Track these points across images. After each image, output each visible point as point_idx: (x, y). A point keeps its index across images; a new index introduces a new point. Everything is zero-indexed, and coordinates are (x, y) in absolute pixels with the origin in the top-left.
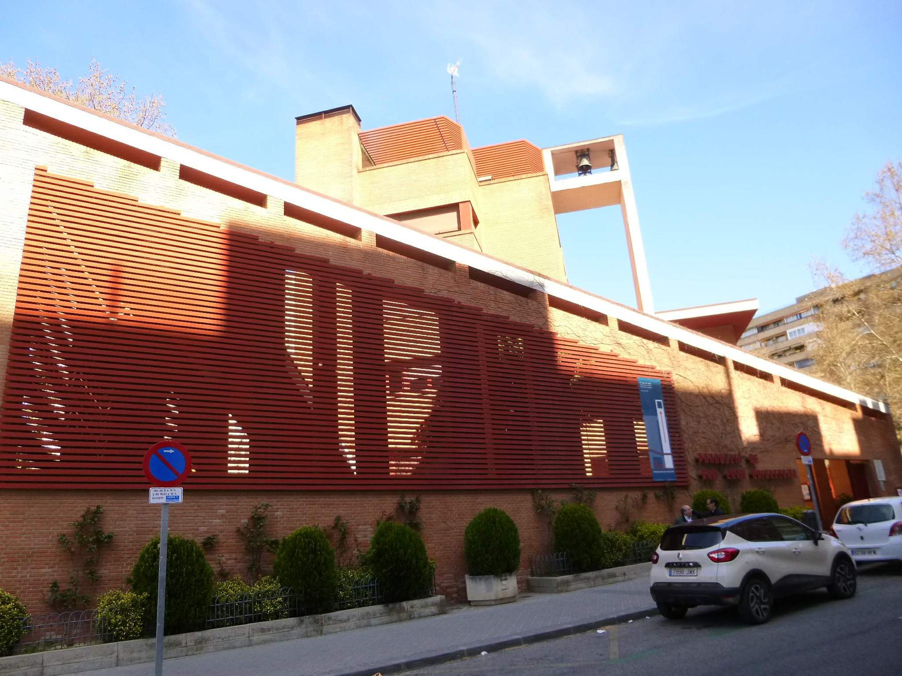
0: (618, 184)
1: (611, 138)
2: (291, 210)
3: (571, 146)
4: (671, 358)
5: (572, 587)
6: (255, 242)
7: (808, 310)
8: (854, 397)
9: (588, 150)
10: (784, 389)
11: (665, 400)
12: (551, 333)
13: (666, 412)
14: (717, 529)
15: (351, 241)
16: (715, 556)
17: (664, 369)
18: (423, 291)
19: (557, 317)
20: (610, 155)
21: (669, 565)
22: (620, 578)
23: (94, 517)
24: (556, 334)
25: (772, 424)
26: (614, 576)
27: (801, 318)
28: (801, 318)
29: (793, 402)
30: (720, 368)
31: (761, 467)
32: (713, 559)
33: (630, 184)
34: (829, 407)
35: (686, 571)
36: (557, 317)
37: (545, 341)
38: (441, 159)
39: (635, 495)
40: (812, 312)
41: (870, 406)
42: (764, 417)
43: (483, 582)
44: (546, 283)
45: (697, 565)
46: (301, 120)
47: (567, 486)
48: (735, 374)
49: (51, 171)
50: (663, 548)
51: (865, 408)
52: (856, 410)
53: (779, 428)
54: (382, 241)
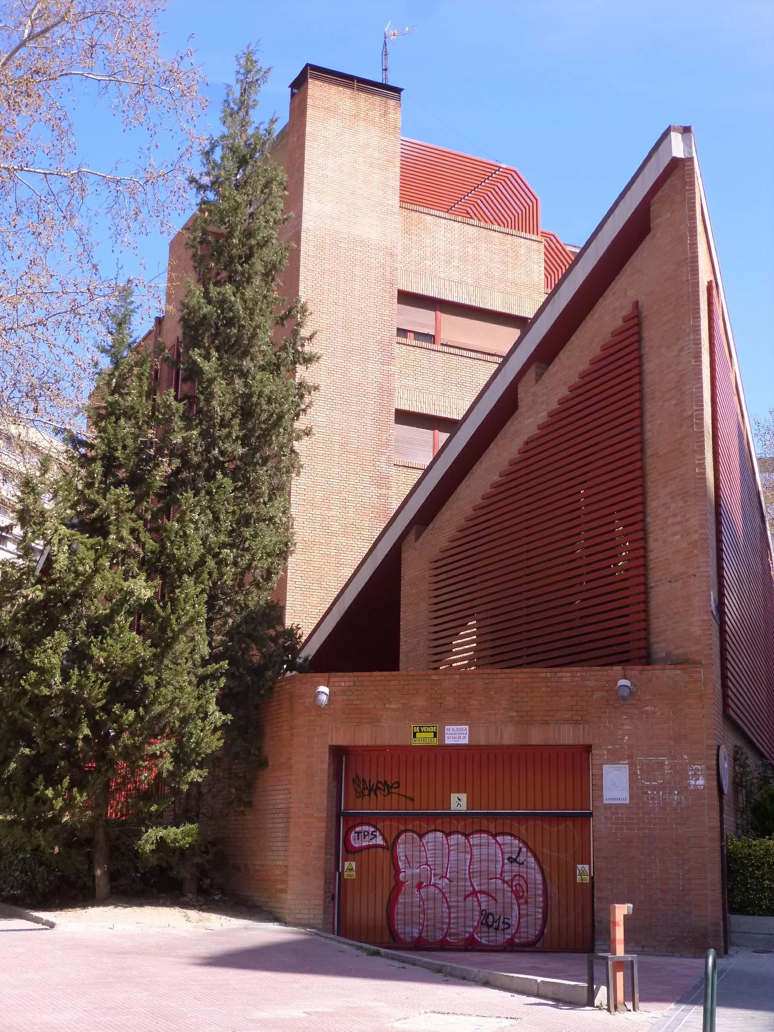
38: (509, 237)
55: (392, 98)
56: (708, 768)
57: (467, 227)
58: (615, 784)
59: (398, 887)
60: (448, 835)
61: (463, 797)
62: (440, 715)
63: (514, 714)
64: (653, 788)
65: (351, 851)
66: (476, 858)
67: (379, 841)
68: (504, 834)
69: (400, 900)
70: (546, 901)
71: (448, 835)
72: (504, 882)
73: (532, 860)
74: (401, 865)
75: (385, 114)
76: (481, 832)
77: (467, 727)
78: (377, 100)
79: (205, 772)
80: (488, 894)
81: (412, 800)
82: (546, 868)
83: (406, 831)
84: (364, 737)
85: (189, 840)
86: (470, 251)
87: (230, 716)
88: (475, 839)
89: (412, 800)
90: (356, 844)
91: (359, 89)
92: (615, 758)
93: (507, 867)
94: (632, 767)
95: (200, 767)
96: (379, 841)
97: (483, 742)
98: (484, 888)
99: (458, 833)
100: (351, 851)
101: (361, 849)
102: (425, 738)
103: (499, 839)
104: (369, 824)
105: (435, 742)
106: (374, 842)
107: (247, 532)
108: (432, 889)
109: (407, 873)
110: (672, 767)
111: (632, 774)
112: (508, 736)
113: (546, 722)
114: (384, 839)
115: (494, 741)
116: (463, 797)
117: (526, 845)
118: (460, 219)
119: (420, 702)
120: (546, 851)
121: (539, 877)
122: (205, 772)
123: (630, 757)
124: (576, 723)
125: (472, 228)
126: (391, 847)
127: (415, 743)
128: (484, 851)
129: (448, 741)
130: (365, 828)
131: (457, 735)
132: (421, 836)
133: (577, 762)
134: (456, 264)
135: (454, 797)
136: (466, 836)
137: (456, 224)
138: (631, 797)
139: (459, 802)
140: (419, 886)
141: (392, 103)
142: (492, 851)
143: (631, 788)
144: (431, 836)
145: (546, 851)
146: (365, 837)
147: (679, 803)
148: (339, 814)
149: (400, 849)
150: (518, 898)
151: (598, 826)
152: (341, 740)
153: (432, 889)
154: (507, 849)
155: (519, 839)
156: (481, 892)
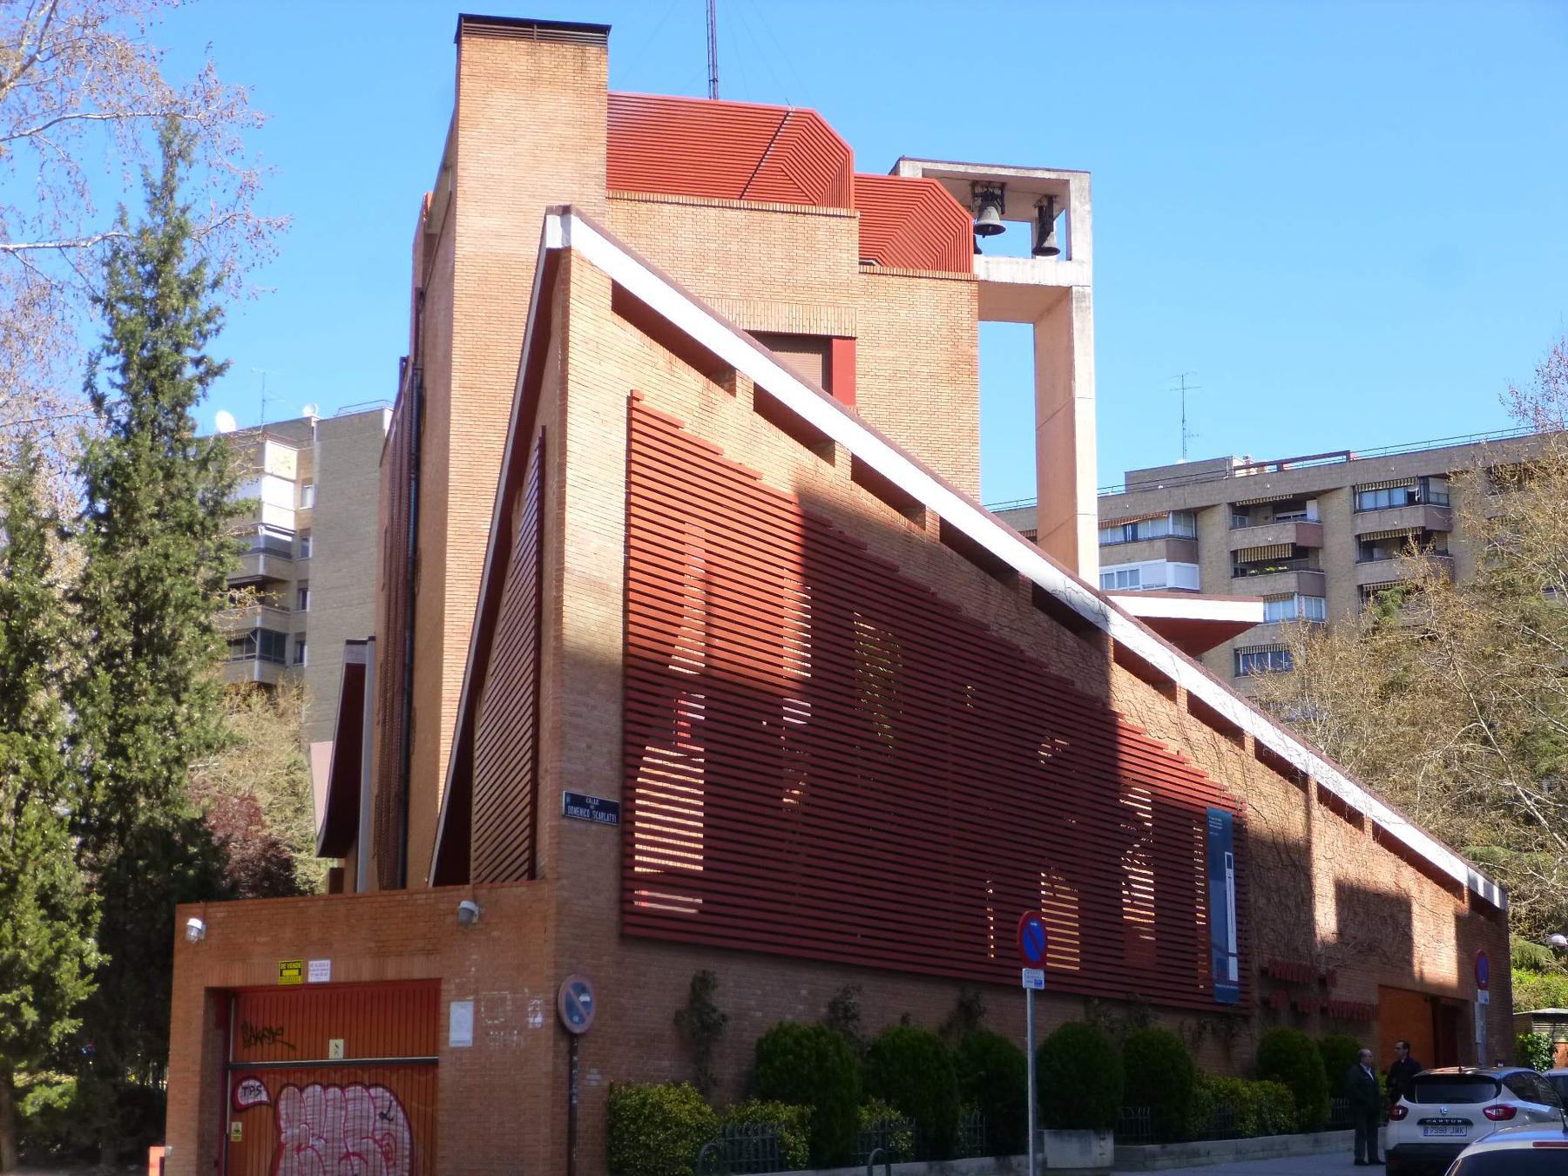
0: (1060, 297)
1: (1065, 176)
2: (863, 474)
3: (971, 170)
4: (1245, 771)
5: (1159, 1164)
6: (824, 530)
7: (1155, 518)
8: (1458, 869)
9: (1003, 186)
10: (1376, 846)
11: (1235, 854)
12: (1115, 714)
13: (1236, 877)
14: (1491, 1080)
15: (901, 521)
16: (1494, 1113)
17: (1236, 792)
18: (985, 627)
19: (1120, 677)
20: (1045, 207)
21: (1422, 1122)
22: (1204, 1160)
23: (702, 985)
24: (1121, 716)
25: (1356, 914)
26: (1196, 1154)
27: (1135, 539)
28: (1135, 539)
29: (1386, 873)
30: (1296, 796)
31: (1340, 993)
32: (1489, 1117)
33: (1090, 302)
34: (1430, 887)
35: (1450, 1130)
36: (1120, 677)
37: (1101, 724)
38: (800, 218)
39: (1191, 1022)
40: (1169, 527)
41: (1481, 892)
42: (1350, 896)
43: (1074, 1139)
44: (1114, 616)
45: (1467, 1123)
46: (472, 25)
47: (1123, 996)
48: (1318, 810)
49: (647, 403)
50: (1410, 1098)
51: (1473, 894)
52: (1461, 898)
53: (1362, 924)
54: (949, 534)
55: (591, 42)
56: (547, 1002)
57: (729, 213)
58: (460, 1023)
59: (279, 1149)
60: (325, 1087)
61: (340, 1042)
62: (304, 951)
63: (372, 945)
64: (496, 1028)
65: (239, 1110)
66: (351, 1115)
67: (264, 1097)
68: (376, 1085)
69: (282, 1165)
70: (412, 1164)
71: (325, 1087)
72: (375, 1141)
73: (401, 1115)
74: (283, 1124)
75: (583, 68)
76: (356, 1083)
77: (327, 962)
78: (568, 50)
79: (79, 1023)
80: (359, 1155)
81: (294, 1048)
82: (414, 1125)
83: (288, 1084)
84: (236, 979)
85: (67, 1099)
86: (734, 247)
87: (108, 957)
88: (351, 1092)
89: (294, 1048)
90: (243, 1101)
91: (542, 38)
92: (461, 996)
93: (378, 1125)
94: (477, 1002)
95: (72, 1016)
96: (264, 1097)
97: (342, 979)
98: (357, 1149)
99: (335, 1085)
100: (239, 1110)
101: (248, 1107)
102: (291, 976)
103: (372, 1091)
104: (255, 1078)
105: (299, 980)
106: (258, 1099)
107: (126, 739)
108: (309, 1151)
109: (288, 1133)
110: (514, 1001)
111: (477, 1012)
112: (366, 971)
113: (400, 954)
114: (268, 1095)
115: (353, 978)
116: (340, 1042)
117: (397, 1099)
118: (716, 202)
119: (288, 934)
120: (415, 1104)
121: (407, 1135)
122: (79, 1023)
123: (476, 992)
124: (429, 953)
125: (738, 212)
126: (274, 1104)
127: (282, 981)
128: (358, 1107)
129: (312, 979)
130: (251, 1082)
131: (319, 971)
132: (301, 1090)
133: (424, 1001)
134: (711, 270)
135: (332, 1043)
136: (342, 1088)
137: (712, 211)
138: (475, 1038)
139: (336, 1050)
140: (299, 1149)
141: (593, 50)
142: (365, 1106)
143: (475, 1029)
144: (310, 1089)
145: (415, 1104)
146: (252, 1094)
147: (518, 1045)
148: (226, 1067)
149: (282, 1105)
150: (388, 1160)
151: (446, 1073)
152: (215, 981)
153: (309, 1151)
154: (379, 1103)
155: (391, 1091)
156: (354, 1154)
